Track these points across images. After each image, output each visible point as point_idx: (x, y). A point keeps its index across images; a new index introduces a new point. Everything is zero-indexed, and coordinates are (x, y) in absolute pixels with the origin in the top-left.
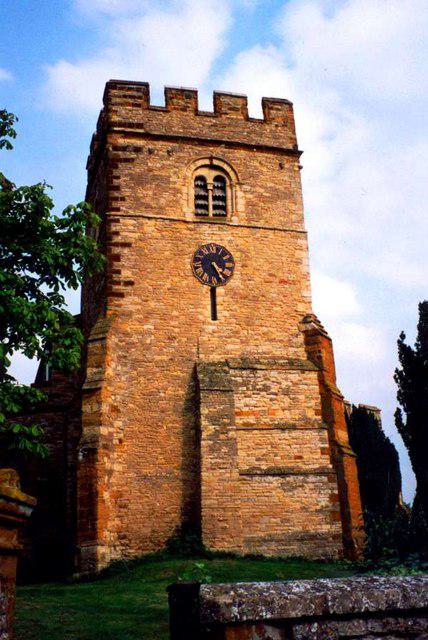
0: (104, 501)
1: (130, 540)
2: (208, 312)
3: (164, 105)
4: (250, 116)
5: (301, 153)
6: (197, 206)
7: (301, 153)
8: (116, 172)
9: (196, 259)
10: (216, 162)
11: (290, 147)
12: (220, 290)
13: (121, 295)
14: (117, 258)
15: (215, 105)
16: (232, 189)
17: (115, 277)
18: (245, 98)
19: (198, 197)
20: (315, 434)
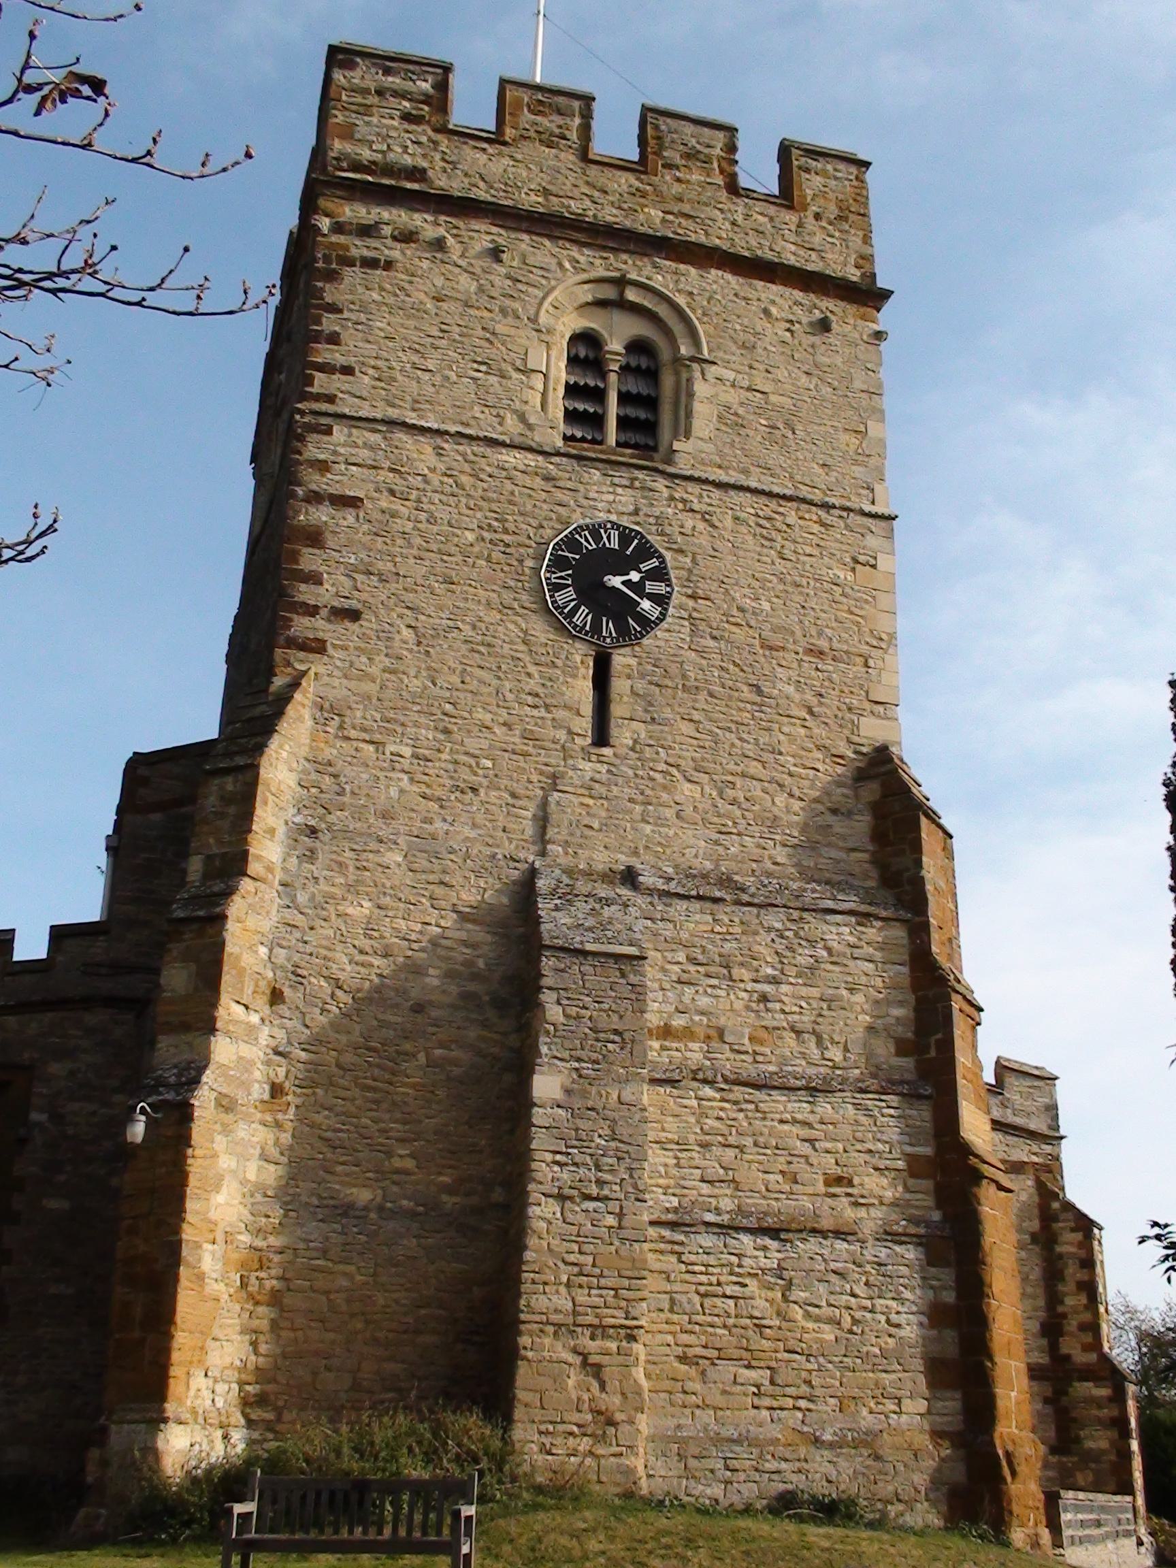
0: (201, 1277)
1: (279, 1412)
2: (584, 724)
3: (636, 158)
4: (744, 181)
5: (886, 295)
6: (571, 416)
7: (886, 295)
8: (331, 293)
9: (558, 563)
10: (631, 295)
11: (854, 275)
12: (621, 660)
13: (318, 647)
14: (315, 538)
15: (642, 141)
16: (677, 374)
17: (305, 593)
18: (731, 131)
19: (572, 391)
20: (222, 1453)
